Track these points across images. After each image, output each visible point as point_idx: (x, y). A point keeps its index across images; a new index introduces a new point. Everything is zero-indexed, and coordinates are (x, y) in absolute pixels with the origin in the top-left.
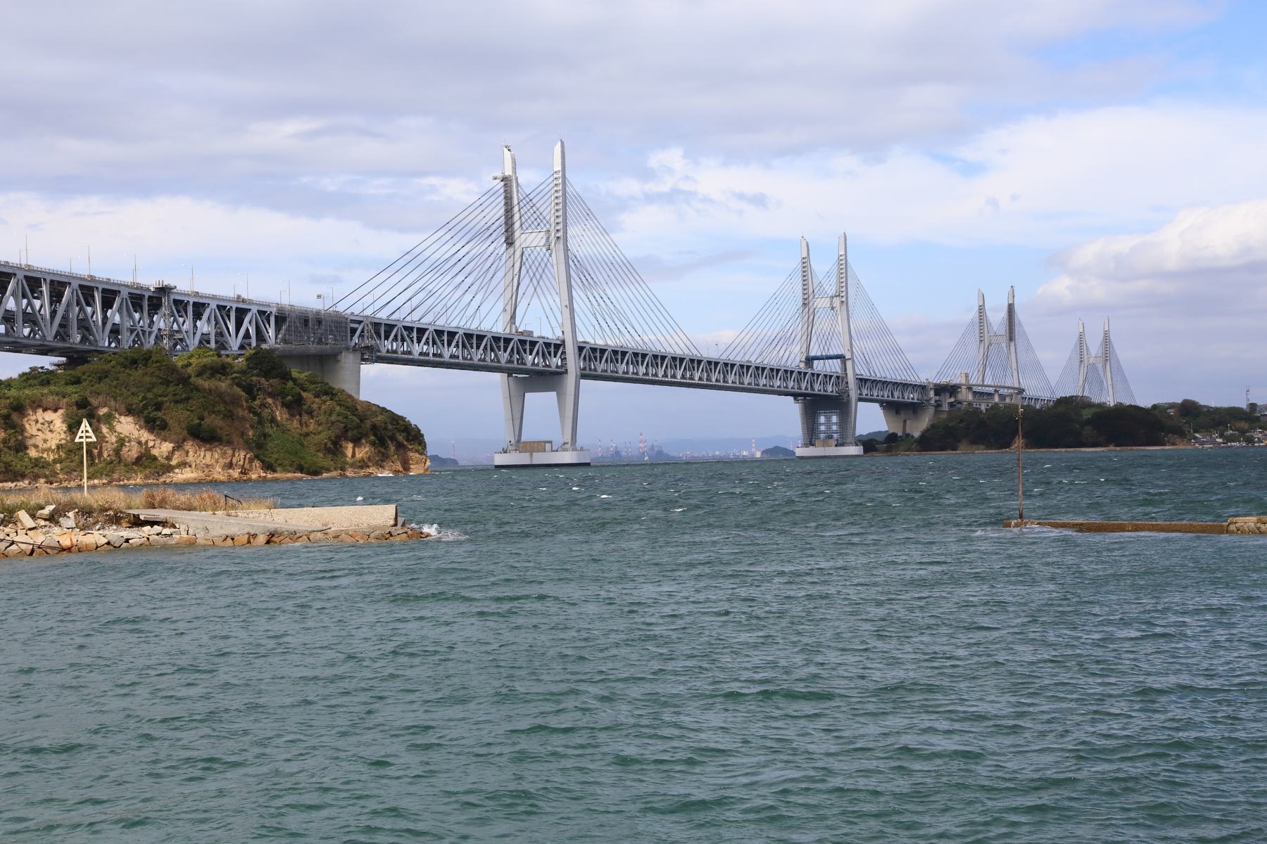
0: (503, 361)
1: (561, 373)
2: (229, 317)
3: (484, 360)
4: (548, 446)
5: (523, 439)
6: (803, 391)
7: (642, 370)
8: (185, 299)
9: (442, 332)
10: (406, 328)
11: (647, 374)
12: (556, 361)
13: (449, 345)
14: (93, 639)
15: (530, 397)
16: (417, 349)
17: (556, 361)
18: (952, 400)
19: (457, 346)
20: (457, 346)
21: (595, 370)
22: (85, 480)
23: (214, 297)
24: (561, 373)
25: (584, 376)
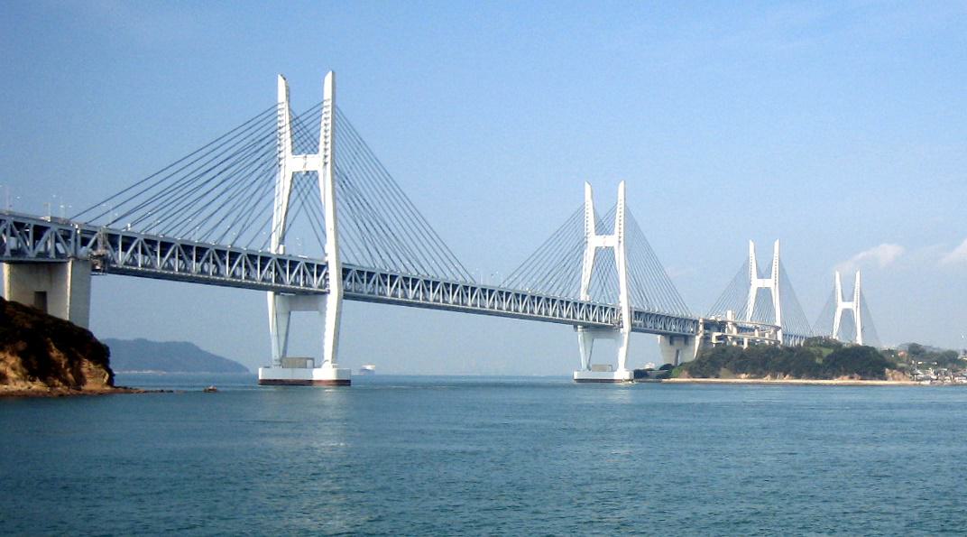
0: (389, 294)
1: (324, 293)
2: (28, 236)
3: (374, 293)
4: (309, 362)
5: (288, 356)
6: (591, 321)
7: (505, 305)
8: (27, 222)
9: (363, 272)
11: (509, 309)
12: (315, 283)
13: (262, 269)
14: (220, 504)
16: (389, 291)
17: (315, 283)
18: (720, 334)
19: (351, 280)
21: (466, 305)
23: (11, 215)
24: (324, 293)
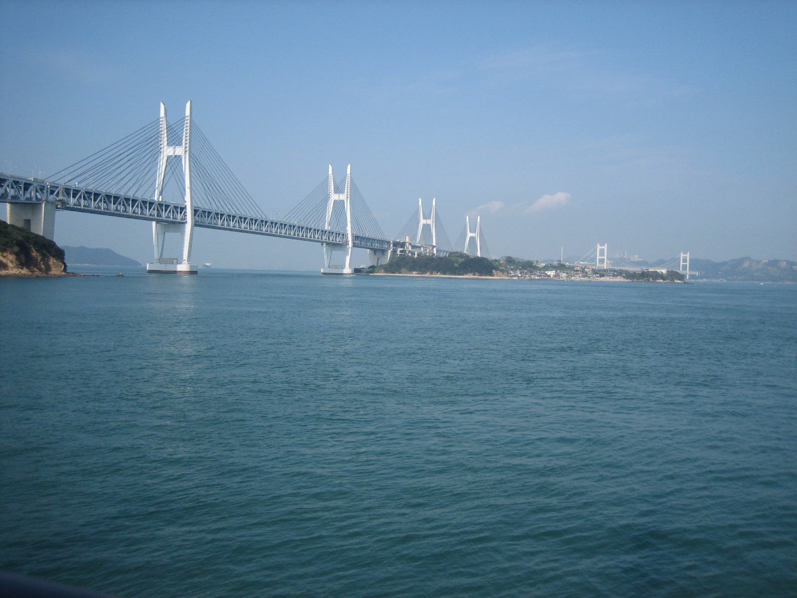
2: (21, 189)
3: (211, 223)
4: (175, 261)
5: (163, 257)
9: (205, 212)
10: (87, 192)
12: (179, 217)
13: (150, 209)
15: (333, 251)
17: (179, 217)
18: (402, 249)
19: (154, 209)
20: (198, 216)
22: (688, 274)
23: (12, 177)
25: (196, 225)
